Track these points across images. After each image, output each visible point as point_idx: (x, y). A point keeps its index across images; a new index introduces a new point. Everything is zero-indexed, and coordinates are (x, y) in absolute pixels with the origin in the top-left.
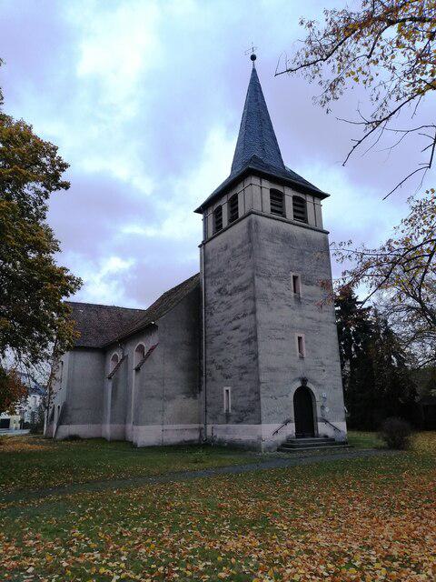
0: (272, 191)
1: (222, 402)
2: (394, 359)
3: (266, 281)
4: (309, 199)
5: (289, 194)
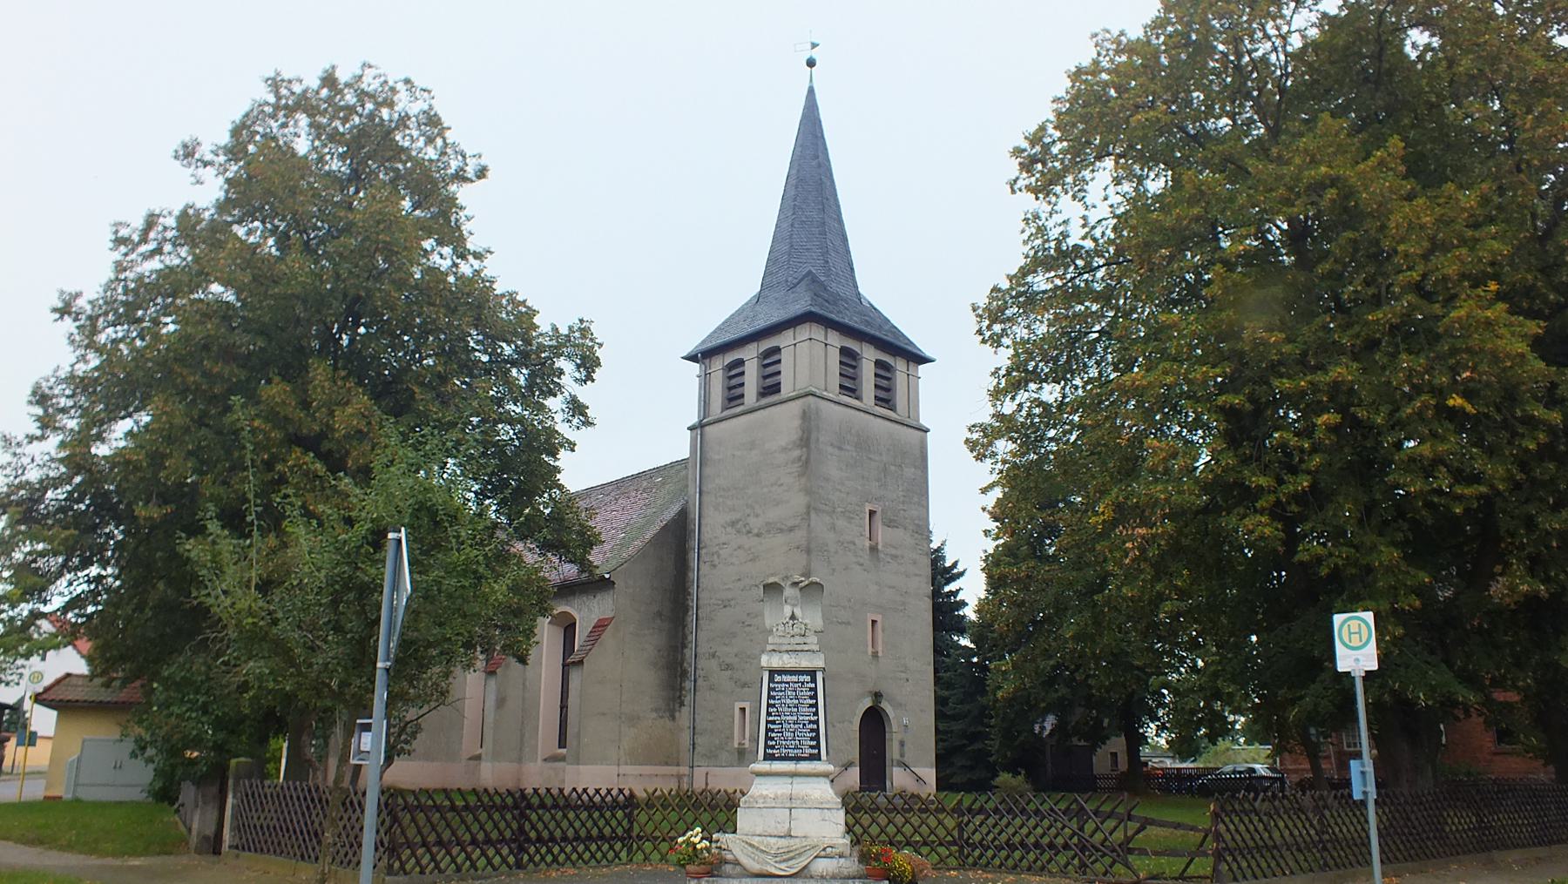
0: (844, 351)
1: (732, 728)
2: (1082, 743)
3: (827, 519)
4: (900, 365)
5: (869, 356)
